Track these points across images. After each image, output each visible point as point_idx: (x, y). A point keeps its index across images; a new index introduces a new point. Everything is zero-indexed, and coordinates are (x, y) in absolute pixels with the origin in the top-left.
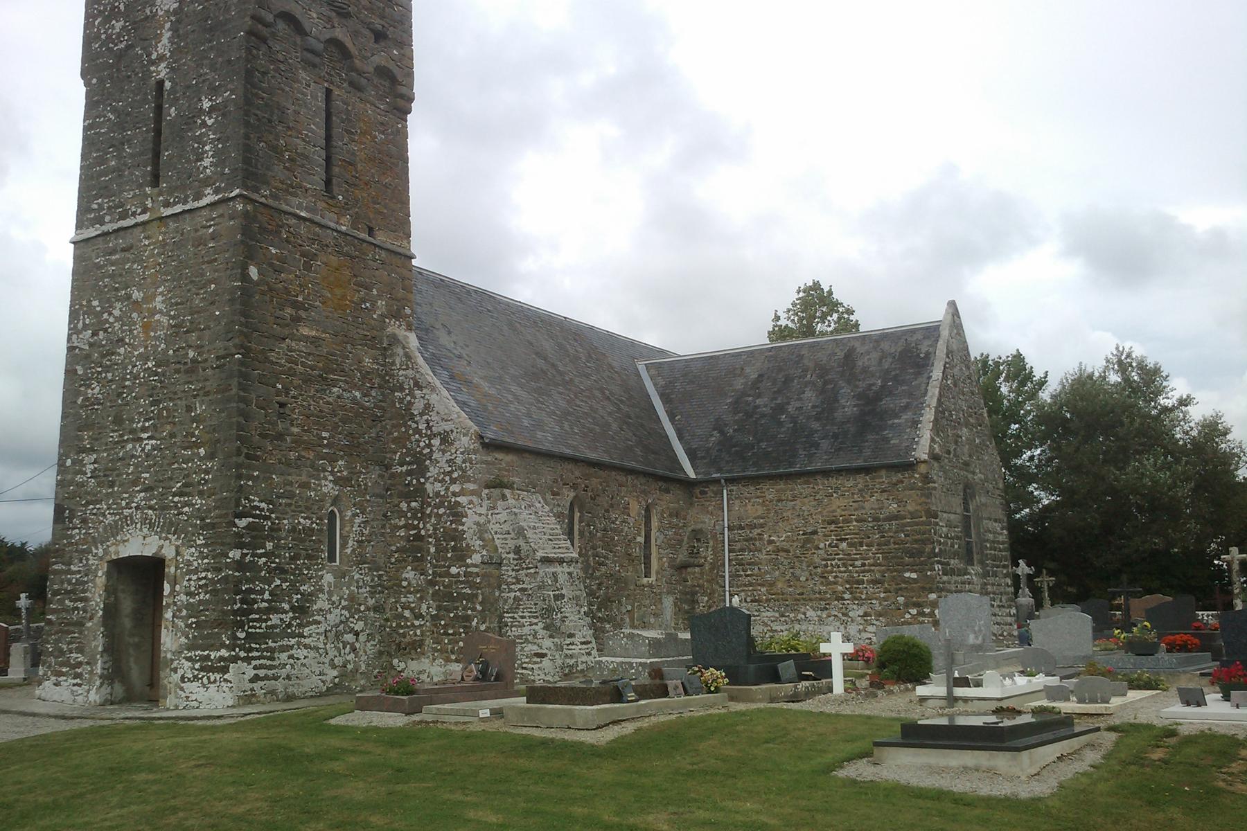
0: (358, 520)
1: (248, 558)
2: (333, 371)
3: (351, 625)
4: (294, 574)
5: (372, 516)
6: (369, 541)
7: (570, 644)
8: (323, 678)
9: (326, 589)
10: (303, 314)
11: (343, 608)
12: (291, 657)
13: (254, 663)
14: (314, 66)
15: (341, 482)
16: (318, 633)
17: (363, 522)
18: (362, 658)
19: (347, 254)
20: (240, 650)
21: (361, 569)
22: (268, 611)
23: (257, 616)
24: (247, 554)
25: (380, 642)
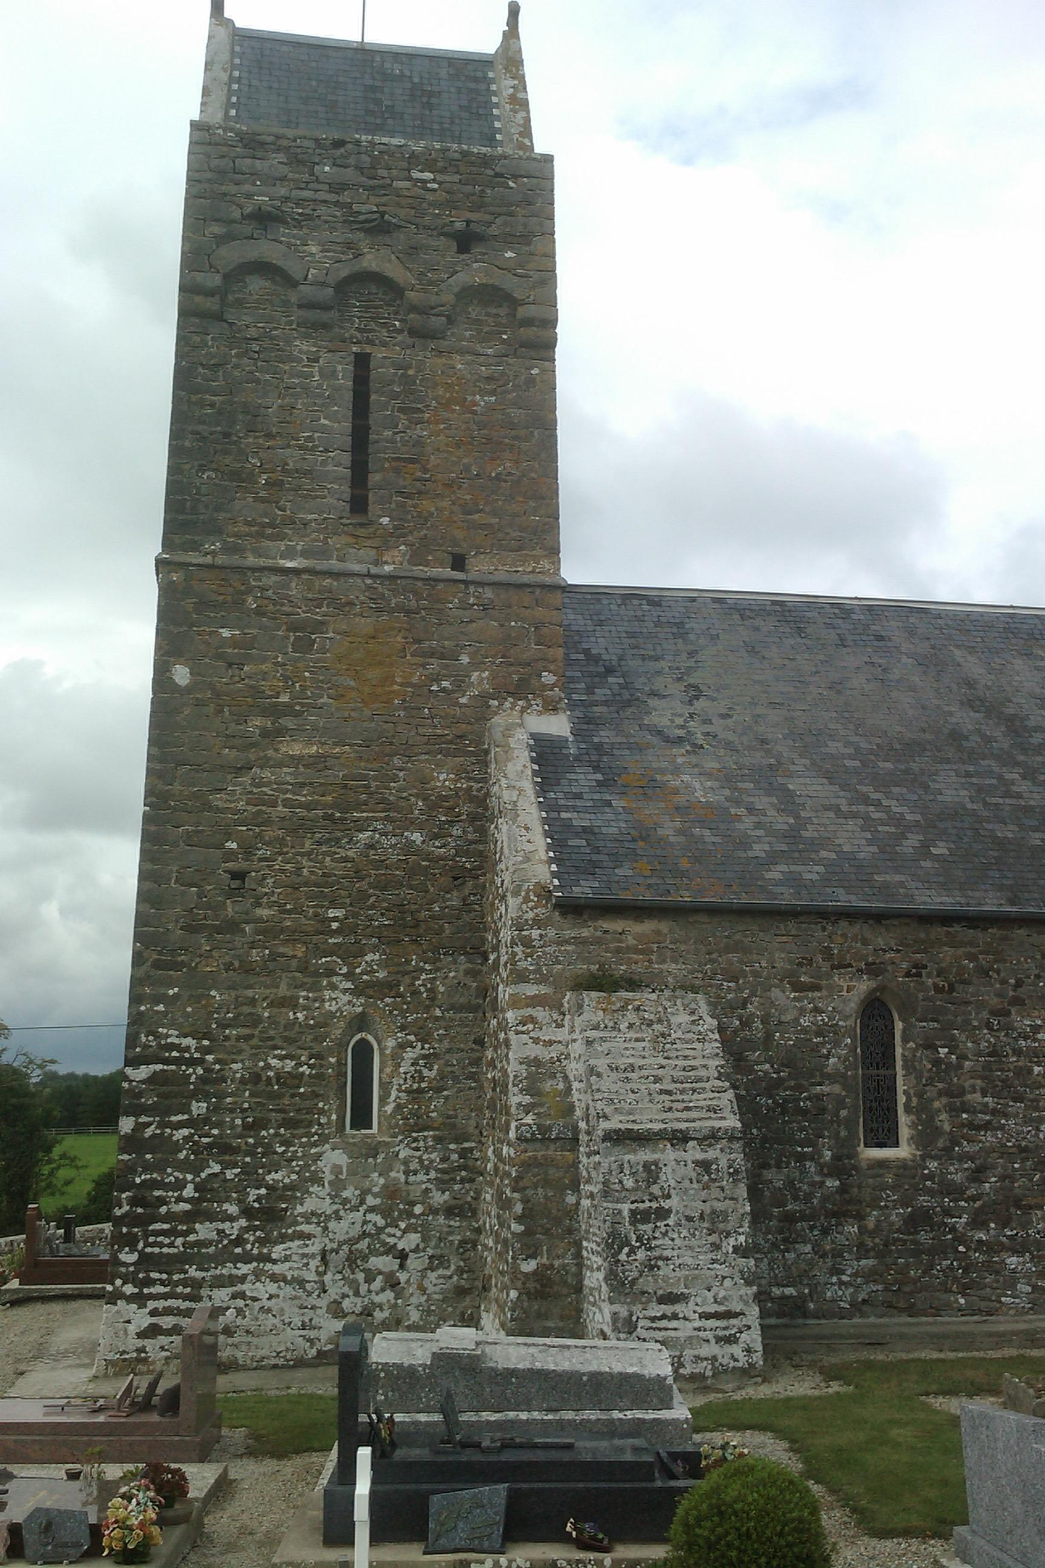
0: (410, 1054)
1: (149, 1132)
2: (359, 806)
3: (388, 1240)
4: (252, 1153)
5: (446, 1044)
6: (439, 1090)
7: (663, 1317)
8: (312, 1334)
9: (328, 1177)
10: (289, 722)
11: (372, 1210)
12: (242, 1295)
13: (151, 1305)
14: (325, 326)
15: (370, 992)
16: (304, 1255)
17: (424, 1057)
18: (414, 1300)
19: (400, 608)
20: (124, 1283)
21: (416, 1140)
22: (190, 1217)
23: (166, 1226)
24: (149, 1124)
25: (460, 1271)
